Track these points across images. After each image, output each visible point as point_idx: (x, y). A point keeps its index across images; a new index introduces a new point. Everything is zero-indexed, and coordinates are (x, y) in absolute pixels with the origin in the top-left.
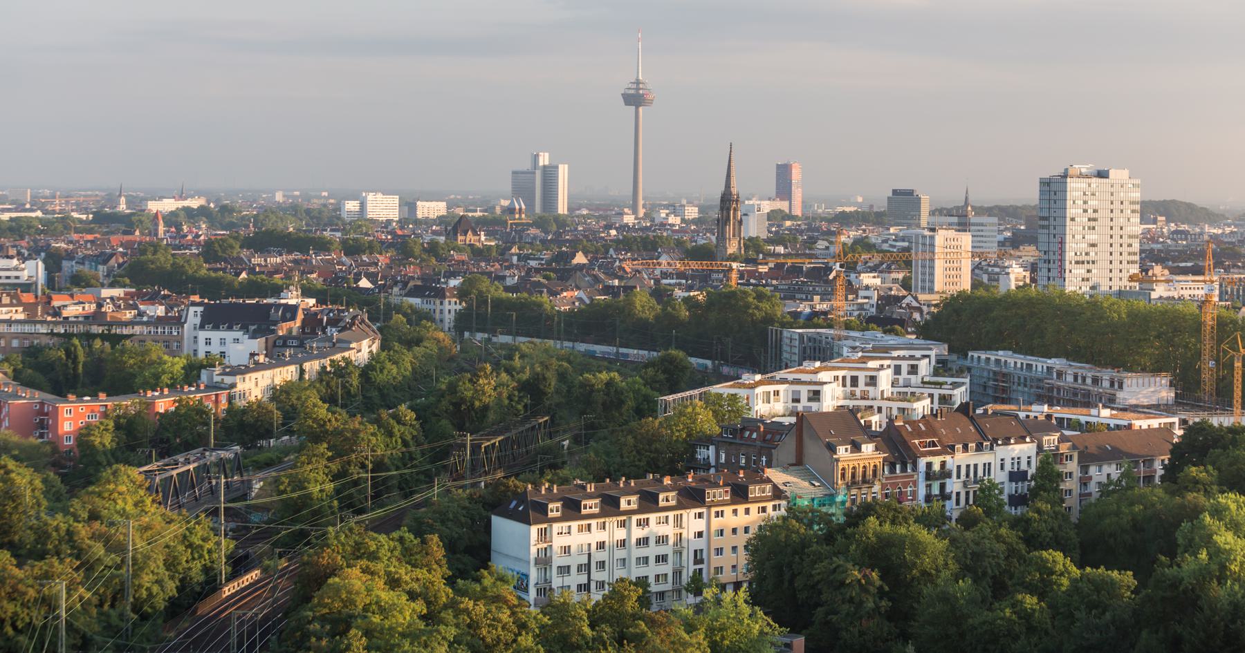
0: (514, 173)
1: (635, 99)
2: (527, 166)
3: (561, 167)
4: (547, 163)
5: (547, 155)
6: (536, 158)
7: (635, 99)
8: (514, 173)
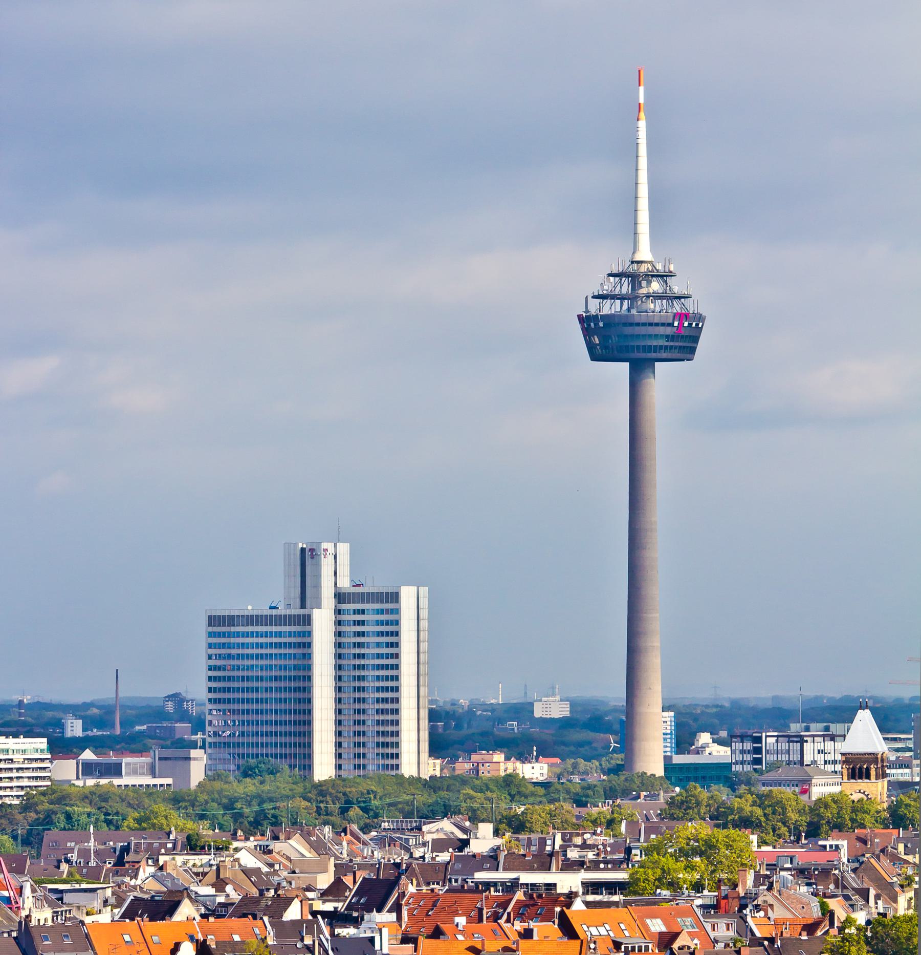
0: (213, 620)
1: (634, 336)
2: (270, 593)
3: (408, 595)
4: (345, 583)
5: (344, 549)
6: (307, 559)
7: (634, 336)
8: (213, 620)
